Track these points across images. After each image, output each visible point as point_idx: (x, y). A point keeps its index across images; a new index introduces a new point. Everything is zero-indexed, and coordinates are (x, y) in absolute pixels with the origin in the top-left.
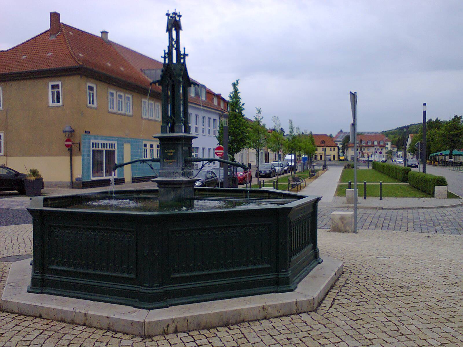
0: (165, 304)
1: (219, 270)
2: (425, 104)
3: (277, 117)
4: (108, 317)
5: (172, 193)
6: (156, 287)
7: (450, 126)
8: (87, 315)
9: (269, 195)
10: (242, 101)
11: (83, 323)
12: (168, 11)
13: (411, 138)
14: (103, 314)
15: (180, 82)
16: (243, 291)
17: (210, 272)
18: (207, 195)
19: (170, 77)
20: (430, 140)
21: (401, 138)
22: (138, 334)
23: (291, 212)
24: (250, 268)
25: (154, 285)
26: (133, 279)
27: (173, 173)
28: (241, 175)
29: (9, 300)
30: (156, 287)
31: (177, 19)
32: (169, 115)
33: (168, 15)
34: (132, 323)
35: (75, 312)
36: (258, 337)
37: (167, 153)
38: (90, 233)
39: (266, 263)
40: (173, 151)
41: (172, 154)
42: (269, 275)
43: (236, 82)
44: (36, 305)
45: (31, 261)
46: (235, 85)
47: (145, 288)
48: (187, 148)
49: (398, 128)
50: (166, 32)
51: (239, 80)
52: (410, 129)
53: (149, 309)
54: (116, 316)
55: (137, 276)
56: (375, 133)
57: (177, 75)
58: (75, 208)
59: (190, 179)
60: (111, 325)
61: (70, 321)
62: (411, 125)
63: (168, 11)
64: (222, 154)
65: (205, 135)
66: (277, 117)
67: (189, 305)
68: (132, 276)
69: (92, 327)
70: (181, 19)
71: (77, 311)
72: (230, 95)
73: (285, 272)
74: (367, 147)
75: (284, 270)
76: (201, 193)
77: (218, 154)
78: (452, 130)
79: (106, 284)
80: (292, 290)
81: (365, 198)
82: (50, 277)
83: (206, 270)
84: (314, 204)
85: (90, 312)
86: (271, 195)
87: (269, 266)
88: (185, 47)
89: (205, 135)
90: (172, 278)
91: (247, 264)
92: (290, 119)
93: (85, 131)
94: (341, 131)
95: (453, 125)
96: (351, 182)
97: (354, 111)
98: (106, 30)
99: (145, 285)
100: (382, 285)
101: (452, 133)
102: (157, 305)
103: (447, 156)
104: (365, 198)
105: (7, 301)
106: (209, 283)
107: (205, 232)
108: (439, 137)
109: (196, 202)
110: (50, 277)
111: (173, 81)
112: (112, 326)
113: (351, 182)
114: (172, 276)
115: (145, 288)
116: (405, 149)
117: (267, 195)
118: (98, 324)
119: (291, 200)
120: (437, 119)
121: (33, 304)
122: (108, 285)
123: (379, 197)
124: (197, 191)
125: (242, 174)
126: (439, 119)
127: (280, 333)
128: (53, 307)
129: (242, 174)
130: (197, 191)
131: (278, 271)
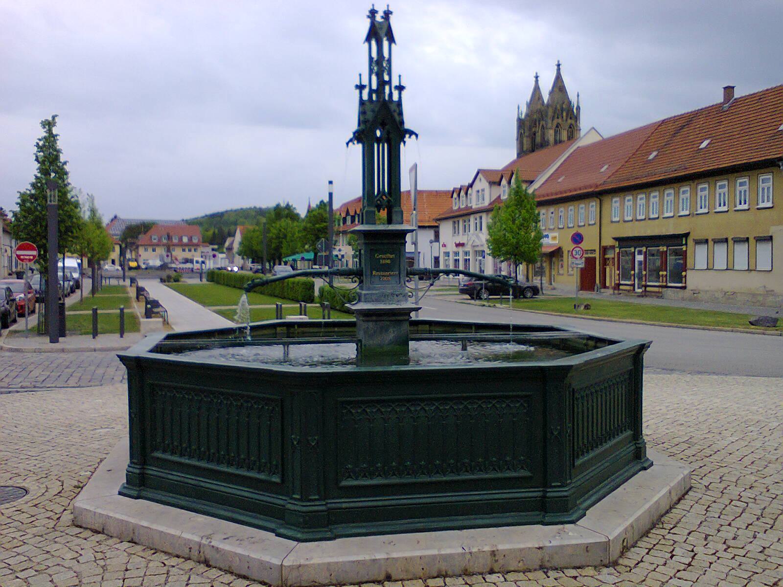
2: (331, 182)
3: (80, 190)
4: (540, 548)
5: (391, 330)
7: (314, 216)
8: (496, 553)
9: (288, 330)
10: (62, 158)
11: (488, 570)
12: (388, 6)
13: (241, 234)
14: (530, 546)
18: (434, 332)
20: (281, 236)
21: (216, 231)
22: (599, 562)
26: (277, 484)
27: (392, 294)
28: (20, 298)
29: (302, 562)
34: (587, 548)
35: (471, 553)
37: (379, 259)
40: (391, 256)
41: (388, 261)
43: (50, 119)
44: (377, 557)
46: (49, 125)
49: (206, 216)
50: (364, 43)
51: (56, 116)
52: (226, 217)
54: (554, 543)
55: (283, 481)
60: (547, 559)
61: (458, 571)
62: (227, 211)
64: (32, 257)
66: (80, 190)
68: (276, 479)
69: (510, 572)
71: (474, 550)
72: (38, 144)
73: (559, 486)
74: (152, 245)
76: (301, 329)
77: (22, 257)
78: (317, 223)
79: (475, 496)
81: (122, 336)
82: (152, 471)
85: (501, 547)
86: (432, 328)
87: (527, 474)
88: (362, 74)
92: (90, 194)
94: (116, 217)
95: (319, 214)
96: (96, 309)
99: (553, 484)
101: (317, 226)
103: (310, 262)
104: (122, 336)
105: (300, 566)
108: (299, 232)
109: (412, 344)
110: (152, 471)
112: (548, 561)
113: (96, 309)
114: (344, 483)
116: (230, 249)
117: (427, 327)
118: (519, 565)
120: (288, 205)
121: (368, 558)
122: (477, 498)
123: (91, 334)
124: (296, 327)
125: (22, 295)
126: (290, 204)
128: (418, 553)
129: (22, 295)
130: (296, 327)
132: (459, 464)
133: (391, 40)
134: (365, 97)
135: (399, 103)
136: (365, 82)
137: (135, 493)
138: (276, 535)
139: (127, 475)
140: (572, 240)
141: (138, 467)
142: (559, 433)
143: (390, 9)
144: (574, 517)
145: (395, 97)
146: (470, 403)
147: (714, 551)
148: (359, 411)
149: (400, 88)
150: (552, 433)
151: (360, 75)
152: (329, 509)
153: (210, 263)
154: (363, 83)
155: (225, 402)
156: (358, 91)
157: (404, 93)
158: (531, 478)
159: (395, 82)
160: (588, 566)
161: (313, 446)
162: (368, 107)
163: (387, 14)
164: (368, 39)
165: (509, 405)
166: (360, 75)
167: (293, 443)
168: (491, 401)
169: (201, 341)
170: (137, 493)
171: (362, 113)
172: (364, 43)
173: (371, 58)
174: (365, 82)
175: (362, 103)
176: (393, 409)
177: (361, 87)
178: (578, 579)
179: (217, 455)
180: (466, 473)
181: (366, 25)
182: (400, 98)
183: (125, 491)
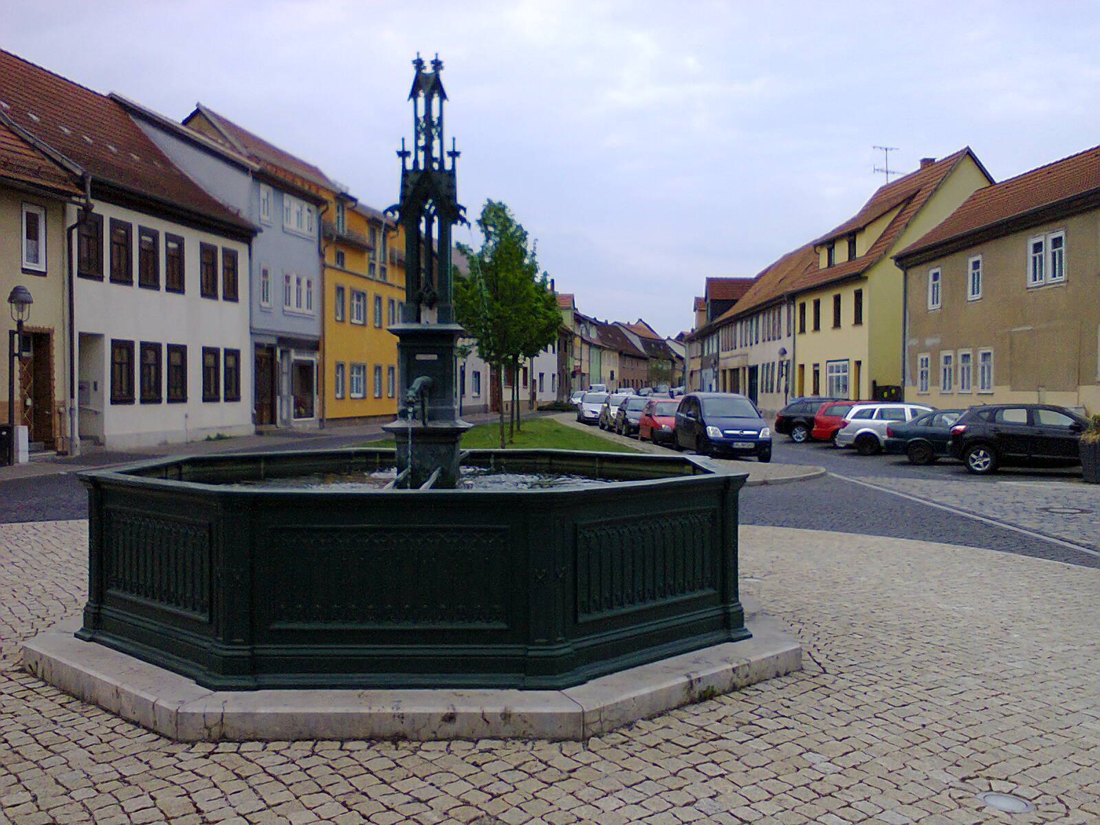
0: (251, 684)
1: (415, 623)
16: (357, 677)
23: (63, 473)
25: (536, 641)
36: (215, 786)
42: (465, 649)
47: (541, 647)
50: (409, 100)
53: (216, 689)
55: (211, 619)
56: (315, 171)
58: (274, 486)
65: (44, 274)
67: (539, 692)
68: (204, 618)
73: (546, 644)
75: (545, 641)
87: (503, 626)
89: (44, 274)
93: (816, 362)
97: (981, 170)
102: (234, 683)
106: (406, 650)
115: (541, 647)
127: (512, 789)
133: (443, 96)
134: (410, 166)
135: (452, 174)
136: (410, 147)
138: (197, 684)
141: (248, 647)
143: (440, 59)
144: (560, 683)
145: (448, 166)
149: (454, 154)
150: (536, 578)
151: (454, 139)
154: (407, 150)
156: (401, 159)
157: (457, 159)
159: (448, 147)
160: (544, 739)
162: (414, 178)
163: (437, 64)
164: (414, 94)
166: (403, 140)
171: (404, 186)
172: (409, 100)
173: (417, 120)
174: (410, 147)
175: (405, 173)
177: (403, 154)
181: (412, 73)
182: (454, 166)
183: (81, 634)
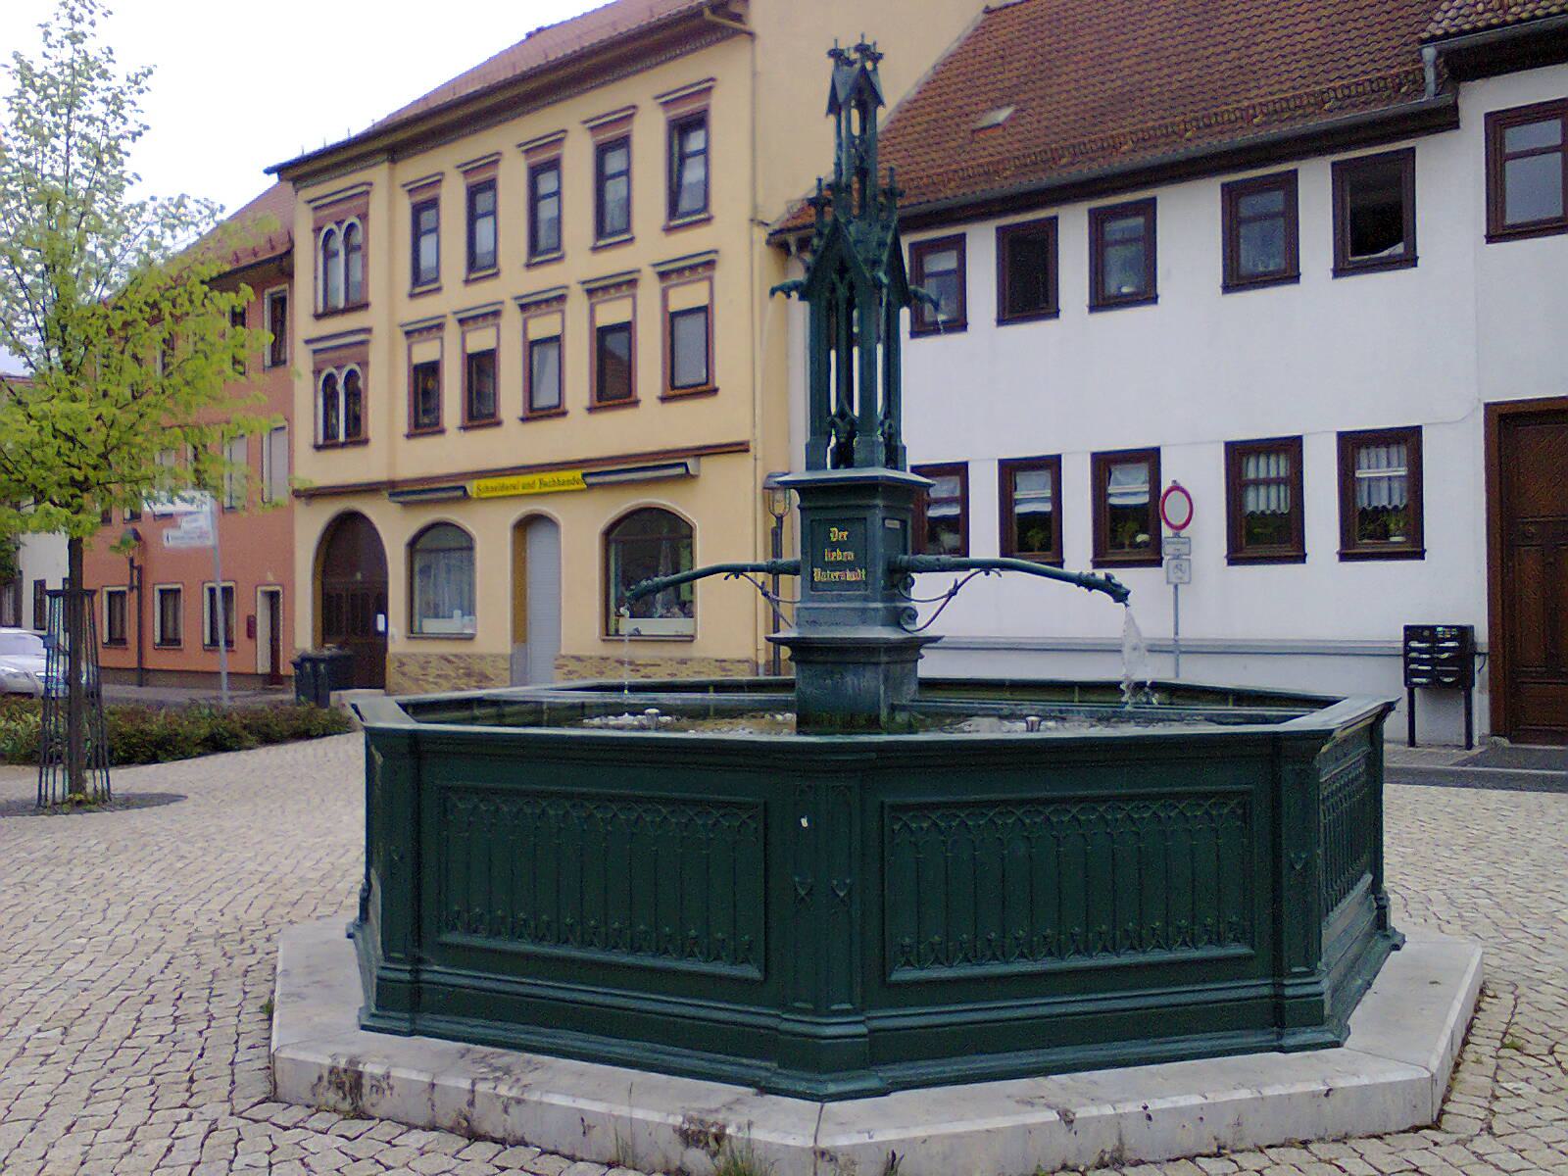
6: (846, 1013)
12: (863, 36)
15: (879, 285)
17: (1114, 960)
19: (843, 270)
24: (1125, 959)
26: (753, 982)
30: (846, 1013)
31: (869, 65)
32: (833, 410)
33: (836, 54)
38: (691, 819)
39: (1236, 940)
45: (348, 924)
48: (896, 524)
55: (766, 970)
57: (866, 261)
59: (909, 635)
63: (863, 36)
68: (753, 972)
70: (881, 65)
80: (1337, 1045)
82: (436, 972)
83: (1128, 949)
84: (1372, 725)
87: (1242, 950)
90: (899, 984)
91: (1003, 954)
98: (566, 128)
100: (307, 1153)
107: (1176, 807)
110: (436, 972)
111: (851, 287)
114: (896, 976)
119: (1297, 711)
131: (1277, 970)
132: (1090, 935)
137: (405, 1026)
139: (378, 985)
140: (691, 528)
142: (1303, 867)
146: (1215, 804)
147: (235, 1166)
148: (1037, 820)
152: (872, 1031)
153: (940, 502)
155: (529, 811)
158: (1250, 958)
161: (842, 901)
165: (937, 825)
167: (797, 894)
168: (1068, 807)
169: (1326, 651)
170: (407, 1024)
176: (1102, 817)
178: (1311, 1147)
179: (603, 930)
180: (1209, 946)
